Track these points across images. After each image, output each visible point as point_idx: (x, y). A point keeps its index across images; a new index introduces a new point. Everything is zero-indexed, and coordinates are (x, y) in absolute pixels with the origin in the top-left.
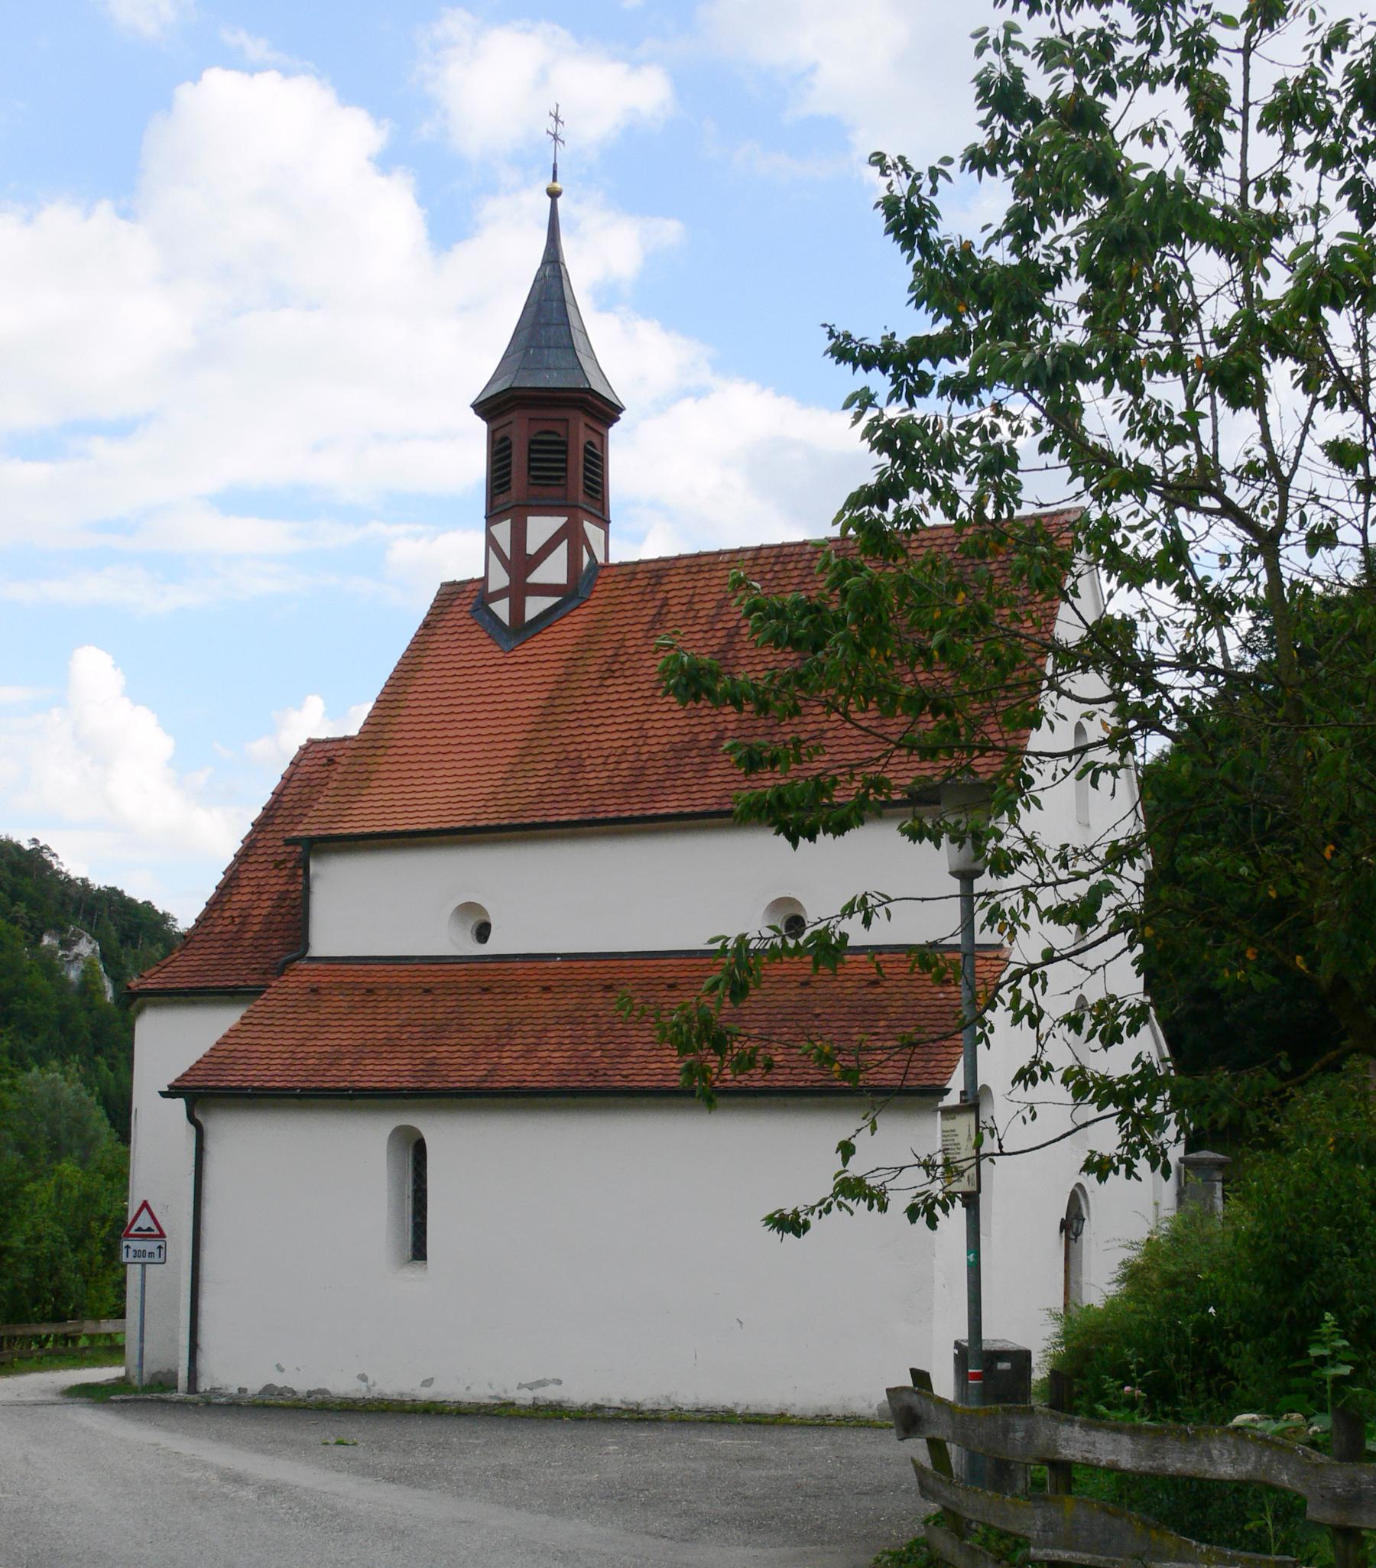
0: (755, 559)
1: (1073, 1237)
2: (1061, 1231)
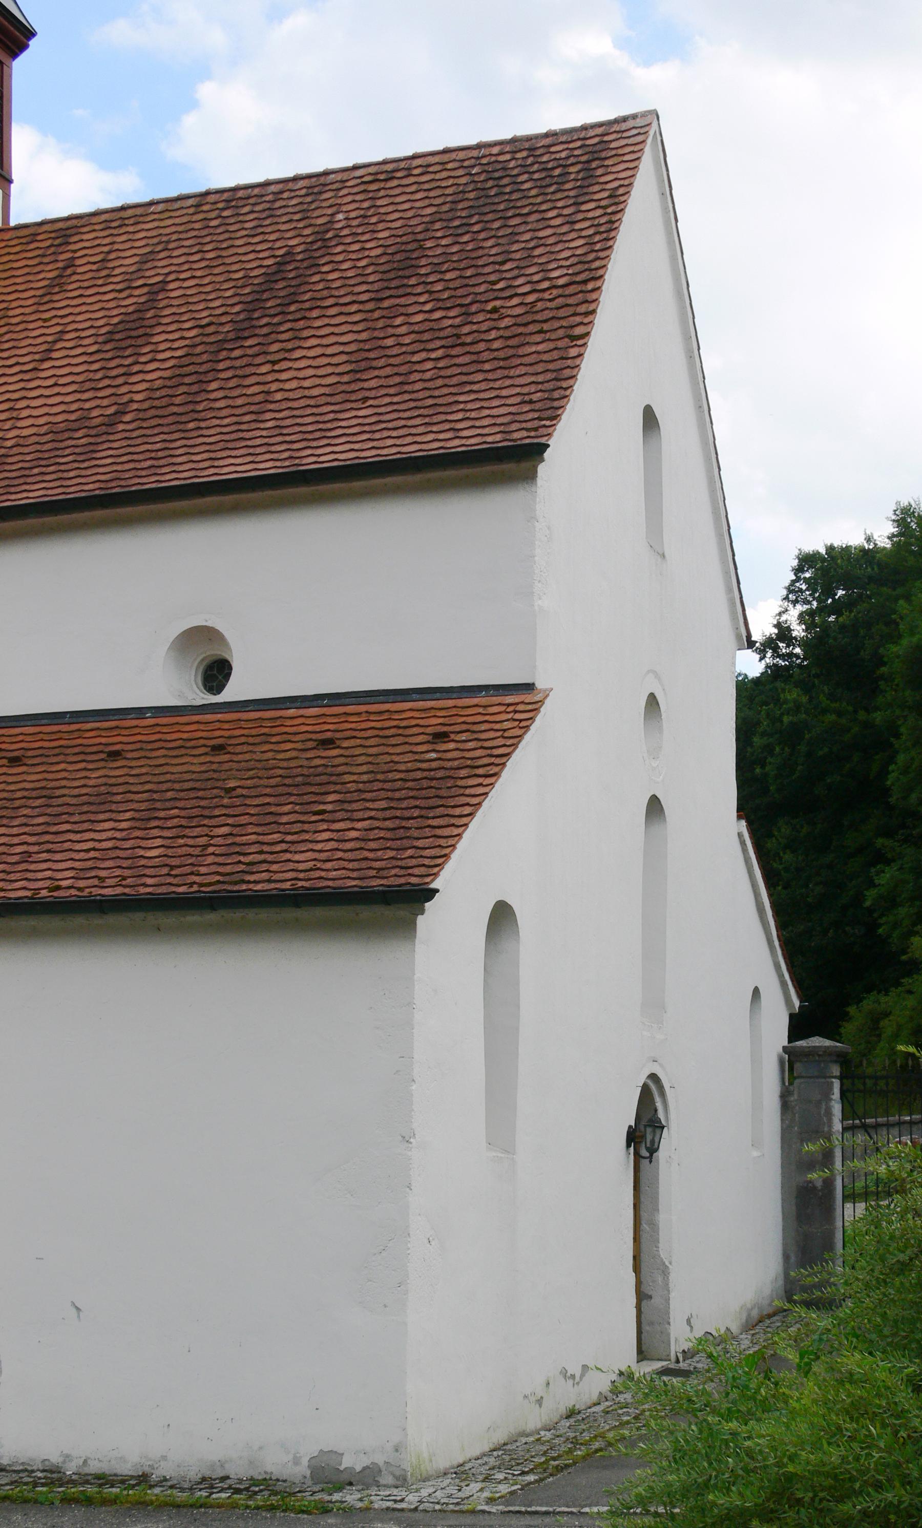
0: (198, 206)
1: (644, 1153)
2: (628, 1146)
